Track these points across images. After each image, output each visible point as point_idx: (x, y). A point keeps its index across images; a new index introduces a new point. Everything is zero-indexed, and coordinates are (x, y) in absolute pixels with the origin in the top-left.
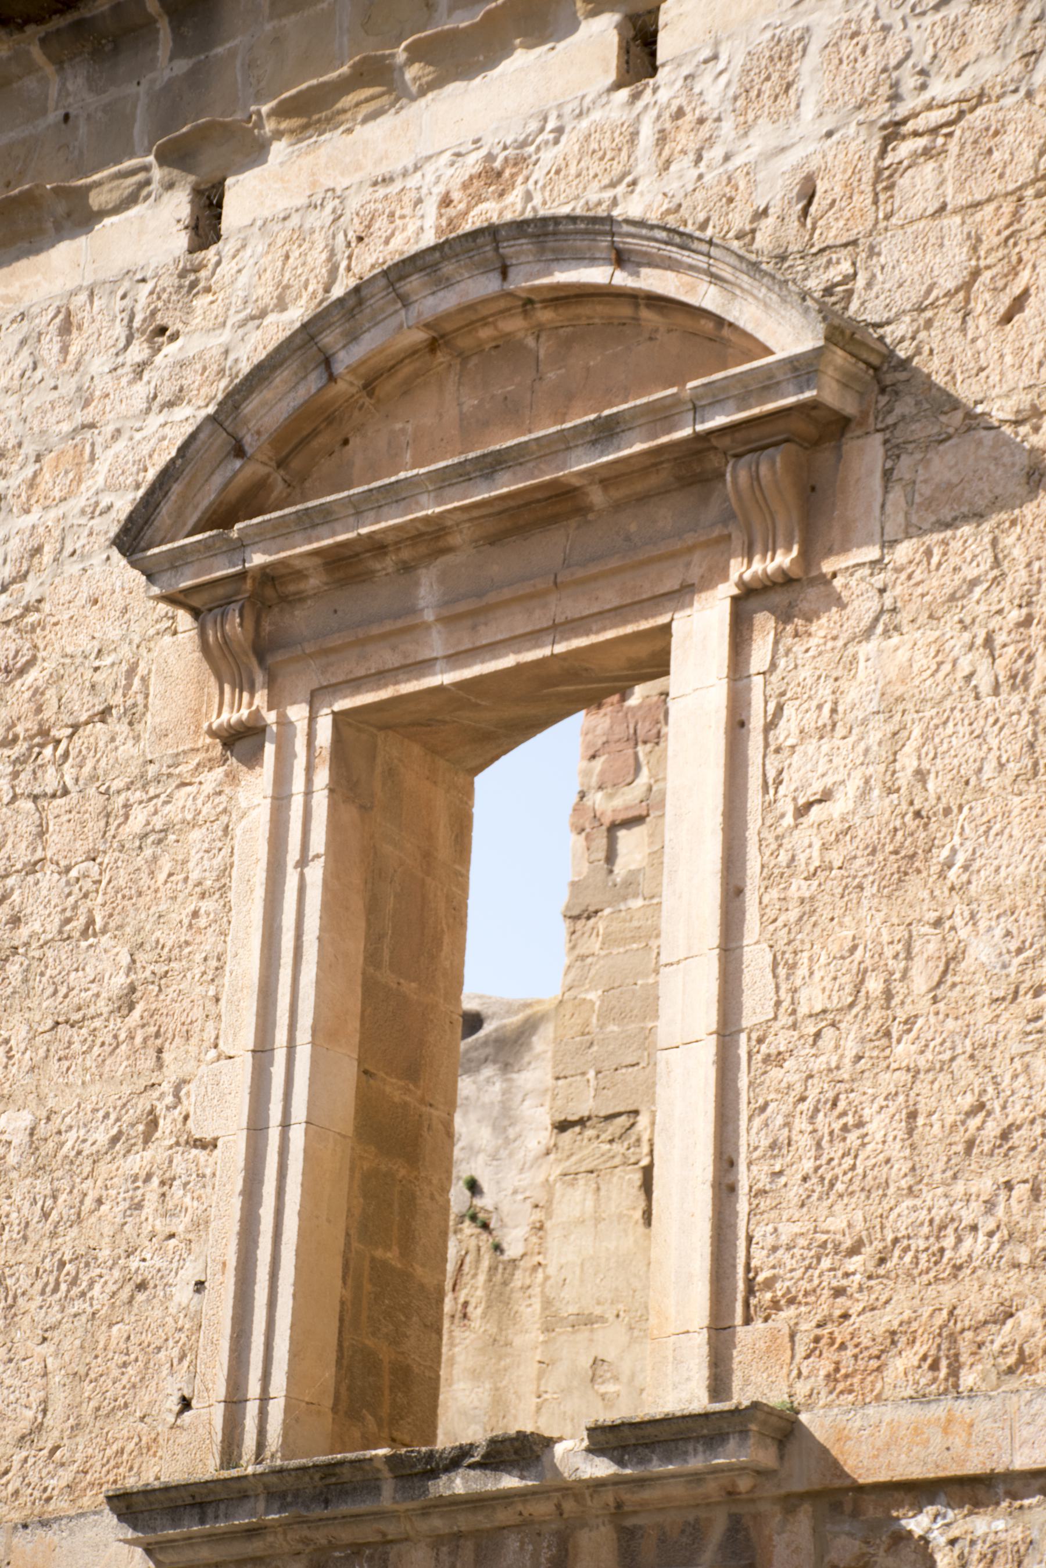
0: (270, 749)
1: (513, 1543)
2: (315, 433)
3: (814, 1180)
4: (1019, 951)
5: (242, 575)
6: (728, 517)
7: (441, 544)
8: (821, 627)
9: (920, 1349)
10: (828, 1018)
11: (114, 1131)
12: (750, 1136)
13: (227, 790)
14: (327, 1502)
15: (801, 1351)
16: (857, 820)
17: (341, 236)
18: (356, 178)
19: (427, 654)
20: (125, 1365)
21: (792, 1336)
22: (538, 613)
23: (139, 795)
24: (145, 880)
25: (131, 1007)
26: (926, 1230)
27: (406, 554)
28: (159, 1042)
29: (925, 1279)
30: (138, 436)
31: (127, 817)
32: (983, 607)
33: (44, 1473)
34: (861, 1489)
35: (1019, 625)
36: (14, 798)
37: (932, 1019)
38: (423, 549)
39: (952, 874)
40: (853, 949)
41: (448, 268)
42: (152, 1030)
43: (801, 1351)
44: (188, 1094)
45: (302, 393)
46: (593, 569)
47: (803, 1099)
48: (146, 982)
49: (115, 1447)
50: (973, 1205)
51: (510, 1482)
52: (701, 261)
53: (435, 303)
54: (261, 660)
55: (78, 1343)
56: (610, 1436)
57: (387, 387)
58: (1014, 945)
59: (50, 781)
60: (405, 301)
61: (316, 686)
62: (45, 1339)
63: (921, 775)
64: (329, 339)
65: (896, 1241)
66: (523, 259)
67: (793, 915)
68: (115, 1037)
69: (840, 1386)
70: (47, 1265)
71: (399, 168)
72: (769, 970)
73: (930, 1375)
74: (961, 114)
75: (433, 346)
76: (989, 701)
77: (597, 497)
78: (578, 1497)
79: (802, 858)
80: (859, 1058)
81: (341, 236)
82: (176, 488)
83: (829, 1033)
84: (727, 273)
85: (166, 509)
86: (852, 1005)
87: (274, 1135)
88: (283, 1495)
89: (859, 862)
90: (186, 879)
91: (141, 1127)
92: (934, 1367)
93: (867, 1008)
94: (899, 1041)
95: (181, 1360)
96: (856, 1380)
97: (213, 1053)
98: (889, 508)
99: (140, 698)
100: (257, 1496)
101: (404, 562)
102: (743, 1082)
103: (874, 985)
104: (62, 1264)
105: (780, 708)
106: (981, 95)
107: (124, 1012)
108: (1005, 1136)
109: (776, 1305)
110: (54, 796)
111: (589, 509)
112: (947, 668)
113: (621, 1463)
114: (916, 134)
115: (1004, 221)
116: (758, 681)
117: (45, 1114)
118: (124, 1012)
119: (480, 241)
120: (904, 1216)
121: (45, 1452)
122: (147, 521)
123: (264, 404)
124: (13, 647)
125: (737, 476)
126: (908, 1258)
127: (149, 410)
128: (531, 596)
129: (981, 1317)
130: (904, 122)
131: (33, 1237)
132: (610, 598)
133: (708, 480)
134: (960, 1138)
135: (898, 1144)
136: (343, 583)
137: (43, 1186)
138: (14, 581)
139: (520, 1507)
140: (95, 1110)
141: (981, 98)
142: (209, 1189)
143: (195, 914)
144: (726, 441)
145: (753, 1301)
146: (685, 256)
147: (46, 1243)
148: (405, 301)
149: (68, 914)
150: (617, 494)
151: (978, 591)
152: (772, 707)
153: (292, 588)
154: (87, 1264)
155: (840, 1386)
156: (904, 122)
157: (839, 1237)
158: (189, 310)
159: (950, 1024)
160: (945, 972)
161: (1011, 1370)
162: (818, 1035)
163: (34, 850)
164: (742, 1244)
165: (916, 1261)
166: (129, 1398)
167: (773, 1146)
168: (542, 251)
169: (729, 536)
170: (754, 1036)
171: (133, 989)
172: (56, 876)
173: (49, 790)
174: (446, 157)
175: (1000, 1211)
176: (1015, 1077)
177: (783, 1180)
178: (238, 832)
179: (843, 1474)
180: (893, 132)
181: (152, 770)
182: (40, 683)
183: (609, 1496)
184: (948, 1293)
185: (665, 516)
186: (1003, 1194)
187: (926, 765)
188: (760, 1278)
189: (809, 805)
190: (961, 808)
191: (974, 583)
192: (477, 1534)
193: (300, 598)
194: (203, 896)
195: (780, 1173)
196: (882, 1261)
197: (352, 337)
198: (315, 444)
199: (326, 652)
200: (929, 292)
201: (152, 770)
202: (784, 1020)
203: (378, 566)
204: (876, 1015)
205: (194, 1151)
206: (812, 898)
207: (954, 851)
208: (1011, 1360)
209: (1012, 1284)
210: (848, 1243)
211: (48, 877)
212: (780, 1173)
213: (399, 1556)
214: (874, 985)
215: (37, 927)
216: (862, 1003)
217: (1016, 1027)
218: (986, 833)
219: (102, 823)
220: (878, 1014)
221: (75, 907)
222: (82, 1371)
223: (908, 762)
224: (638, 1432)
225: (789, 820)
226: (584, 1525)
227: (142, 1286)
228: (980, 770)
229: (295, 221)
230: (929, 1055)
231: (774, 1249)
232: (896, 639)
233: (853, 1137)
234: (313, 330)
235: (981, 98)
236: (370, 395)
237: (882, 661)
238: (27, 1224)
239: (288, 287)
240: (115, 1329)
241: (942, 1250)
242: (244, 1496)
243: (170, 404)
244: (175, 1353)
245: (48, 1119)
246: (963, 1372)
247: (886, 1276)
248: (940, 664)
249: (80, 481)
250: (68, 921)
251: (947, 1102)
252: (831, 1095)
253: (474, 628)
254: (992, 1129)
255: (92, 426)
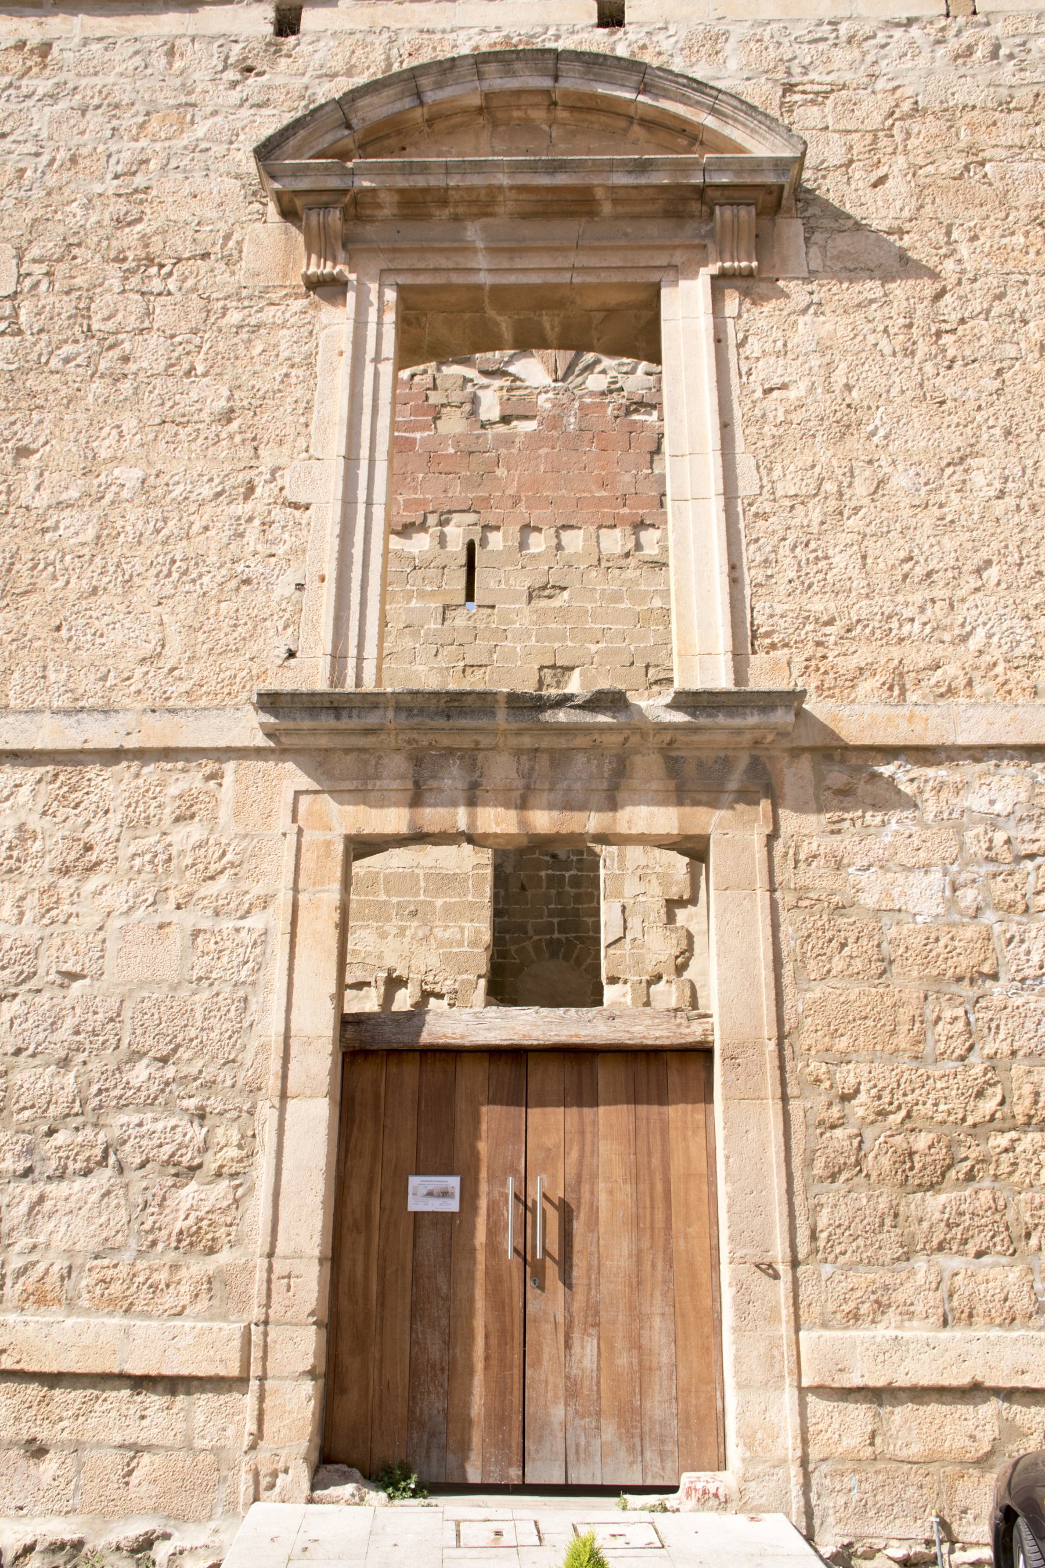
0: (351, 296)
1: (581, 759)
2: (387, 136)
3: (797, 582)
4: (926, 484)
5: (344, 192)
6: (711, 234)
7: (489, 210)
8: (768, 307)
9: (880, 679)
10: (798, 500)
11: (219, 489)
12: (749, 554)
13: (311, 312)
14: (449, 717)
15: (796, 673)
16: (809, 401)
17: (395, 51)
18: (407, 26)
19: (475, 265)
20: (235, 626)
21: (789, 664)
22: (560, 259)
23: (234, 304)
24: (242, 351)
25: (230, 421)
26: (879, 617)
27: (461, 210)
28: (255, 444)
29: (879, 643)
30: (231, 117)
31: (224, 315)
32: (879, 314)
33: (163, 682)
34: (847, 748)
35: (905, 326)
36: (124, 291)
37: (872, 510)
38: (475, 210)
39: (875, 439)
40: (813, 467)
41: (518, 66)
42: (249, 436)
43: (796, 673)
44: (282, 476)
45: (398, 106)
46: (605, 243)
47: (784, 539)
48: (243, 407)
49: (228, 673)
50: (910, 608)
51: (602, 719)
52: (709, 101)
53: (496, 81)
54: (344, 246)
55: (192, 608)
56: (690, 698)
57: (440, 126)
58: (922, 480)
59: (156, 285)
60: (480, 76)
61: (385, 267)
62: (160, 604)
63: (848, 388)
64: (425, 82)
65: (859, 621)
66: (571, 74)
67: (769, 443)
68: (217, 436)
69: (826, 693)
70: (160, 559)
71: (440, 27)
72: (754, 468)
73: (888, 693)
74: (832, 91)
75: (480, 110)
76: (891, 359)
77: (607, 208)
78: (644, 735)
79: (771, 415)
80: (823, 523)
81: (395, 51)
82: (302, 133)
83: (799, 508)
84: (728, 110)
85: (292, 142)
86: (816, 495)
87: (361, 508)
88: (410, 710)
89: (811, 424)
90: (277, 356)
91: (242, 490)
92: (891, 689)
93: (826, 498)
94: (849, 518)
95: (285, 628)
96: (837, 691)
97: (304, 455)
98: (811, 255)
99: (235, 253)
100: (386, 708)
101: (457, 215)
102: (742, 525)
103: (829, 487)
104: (173, 562)
105: (746, 338)
106: (844, 85)
107: (223, 422)
108: (929, 575)
109: (773, 646)
110: (160, 294)
111: (597, 214)
112: (860, 338)
113: (693, 715)
114: (804, 92)
115: (867, 142)
116: (730, 322)
117: (154, 472)
118: (223, 422)
119: (547, 56)
120: (862, 609)
121: (166, 670)
122: (279, 145)
123: (370, 105)
124: (124, 209)
125: (723, 214)
126: (868, 631)
127: (241, 106)
128: (556, 249)
129: (921, 665)
130: (796, 85)
131: (146, 543)
132: (616, 261)
133: (682, 217)
134: (898, 574)
135: (857, 571)
136: (406, 217)
137: (154, 513)
138: (125, 174)
139: (597, 737)
140: (201, 475)
141: (844, 86)
142: (305, 532)
143: (287, 375)
144: (717, 194)
145: (756, 643)
146: (697, 96)
147: (158, 548)
148: (480, 76)
149: (173, 361)
150: (620, 209)
151: (874, 306)
152: (741, 336)
153: (369, 212)
154: (197, 564)
155: (826, 693)
156: (796, 85)
157: (818, 615)
158: (274, 63)
159: (885, 514)
160: (877, 487)
161: (942, 695)
162: (792, 507)
163: (142, 322)
164: (748, 611)
165: (873, 633)
166: (240, 645)
167: (766, 561)
168: (587, 73)
169: (705, 246)
170: (746, 501)
171: (232, 410)
172: (162, 339)
173: (156, 291)
174: (476, 30)
175: (929, 612)
176: (932, 546)
177: (774, 581)
178: (322, 335)
179: (839, 738)
180: (789, 88)
181: (245, 293)
182: (148, 230)
183: (667, 737)
184: (896, 652)
185: (653, 229)
186: (929, 605)
187: (852, 382)
188: (762, 630)
189: (771, 390)
190: (878, 407)
191: (872, 301)
192: (551, 751)
193: (371, 220)
194: (292, 366)
195: (772, 576)
196: (849, 631)
197: (439, 86)
198: (386, 143)
199: (395, 250)
200: (823, 162)
201: (245, 293)
202: (766, 495)
203: (437, 213)
204: (832, 503)
205: (289, 510)
206: (780, 437)
207: (877, 428)
208: (943, 690)
209: (939, 651)
210: (825, 618)
211: (154, 340)
212: (772, 576)
213: (486, 758)
214: (829, 487)
215: (145, 365)
216: (822, 495)
217: (928, 522)
218: (898, 422)
219: (204, 315)
220: (834, 502)
221: (179, 358)
222: (197, 625)
223: (839, 378)
224: (714, 698)
225: (759, 394)
226: (638, 752)
227: (247, 582)
228: (888, 391)
229: (358, 36)
230: (872, 526)
231: (772, 616)
232: (822, 318)
233: (822, 564)
234: (417, 73)
235: (844, 86)
236: (430, 126)
237: (828, 325)
238: (141, 535)
239: (354, 66)
240: (223, 605)
241: (890, 629)
242: (375, 706)
243: (259, 106)
244: (281, 624)
245: (157, 476)
246: (908, 694)
247: (853, 639)
248: (856, 335)
249: (182, 132)
250: (172, 365)
251: (887, 553)
252: (805, 539)
253: (511, 258)
254: (919, 571)
255: (194, 105)
